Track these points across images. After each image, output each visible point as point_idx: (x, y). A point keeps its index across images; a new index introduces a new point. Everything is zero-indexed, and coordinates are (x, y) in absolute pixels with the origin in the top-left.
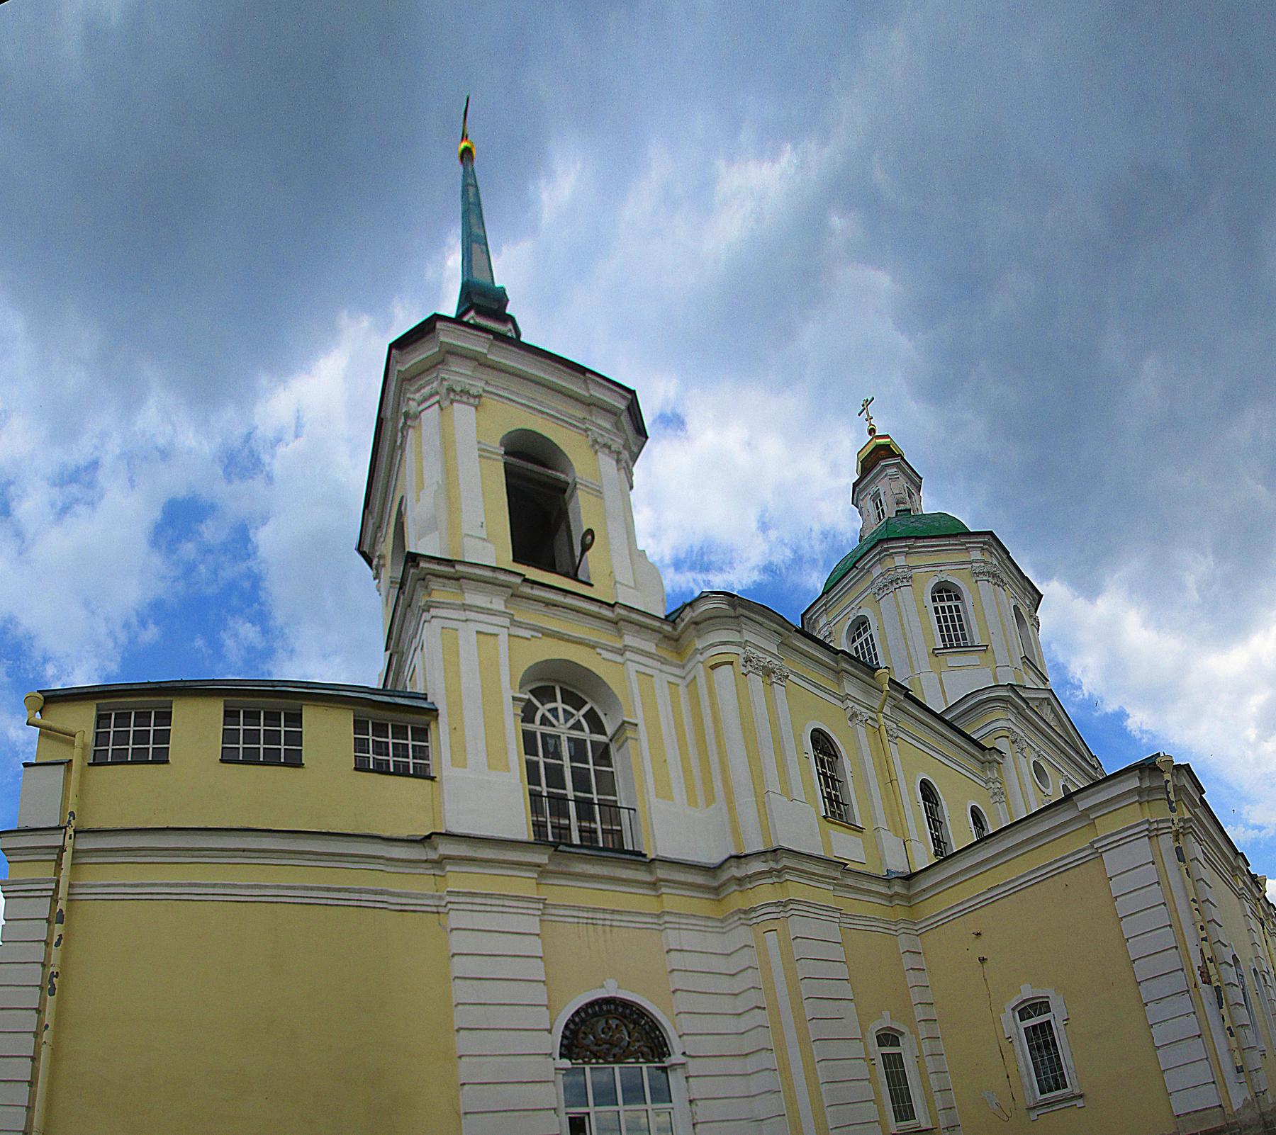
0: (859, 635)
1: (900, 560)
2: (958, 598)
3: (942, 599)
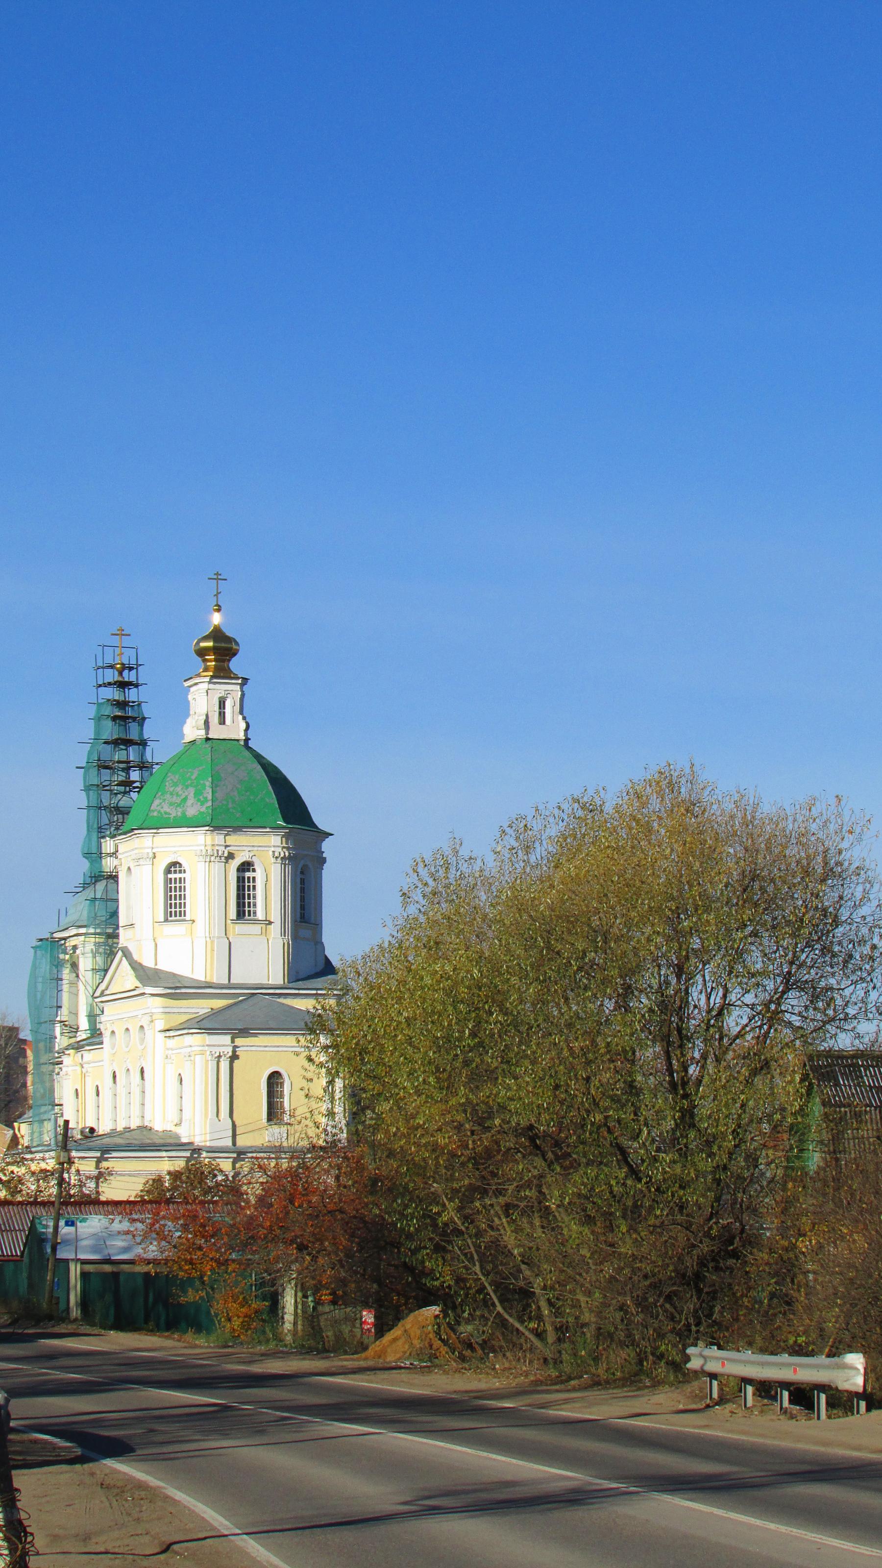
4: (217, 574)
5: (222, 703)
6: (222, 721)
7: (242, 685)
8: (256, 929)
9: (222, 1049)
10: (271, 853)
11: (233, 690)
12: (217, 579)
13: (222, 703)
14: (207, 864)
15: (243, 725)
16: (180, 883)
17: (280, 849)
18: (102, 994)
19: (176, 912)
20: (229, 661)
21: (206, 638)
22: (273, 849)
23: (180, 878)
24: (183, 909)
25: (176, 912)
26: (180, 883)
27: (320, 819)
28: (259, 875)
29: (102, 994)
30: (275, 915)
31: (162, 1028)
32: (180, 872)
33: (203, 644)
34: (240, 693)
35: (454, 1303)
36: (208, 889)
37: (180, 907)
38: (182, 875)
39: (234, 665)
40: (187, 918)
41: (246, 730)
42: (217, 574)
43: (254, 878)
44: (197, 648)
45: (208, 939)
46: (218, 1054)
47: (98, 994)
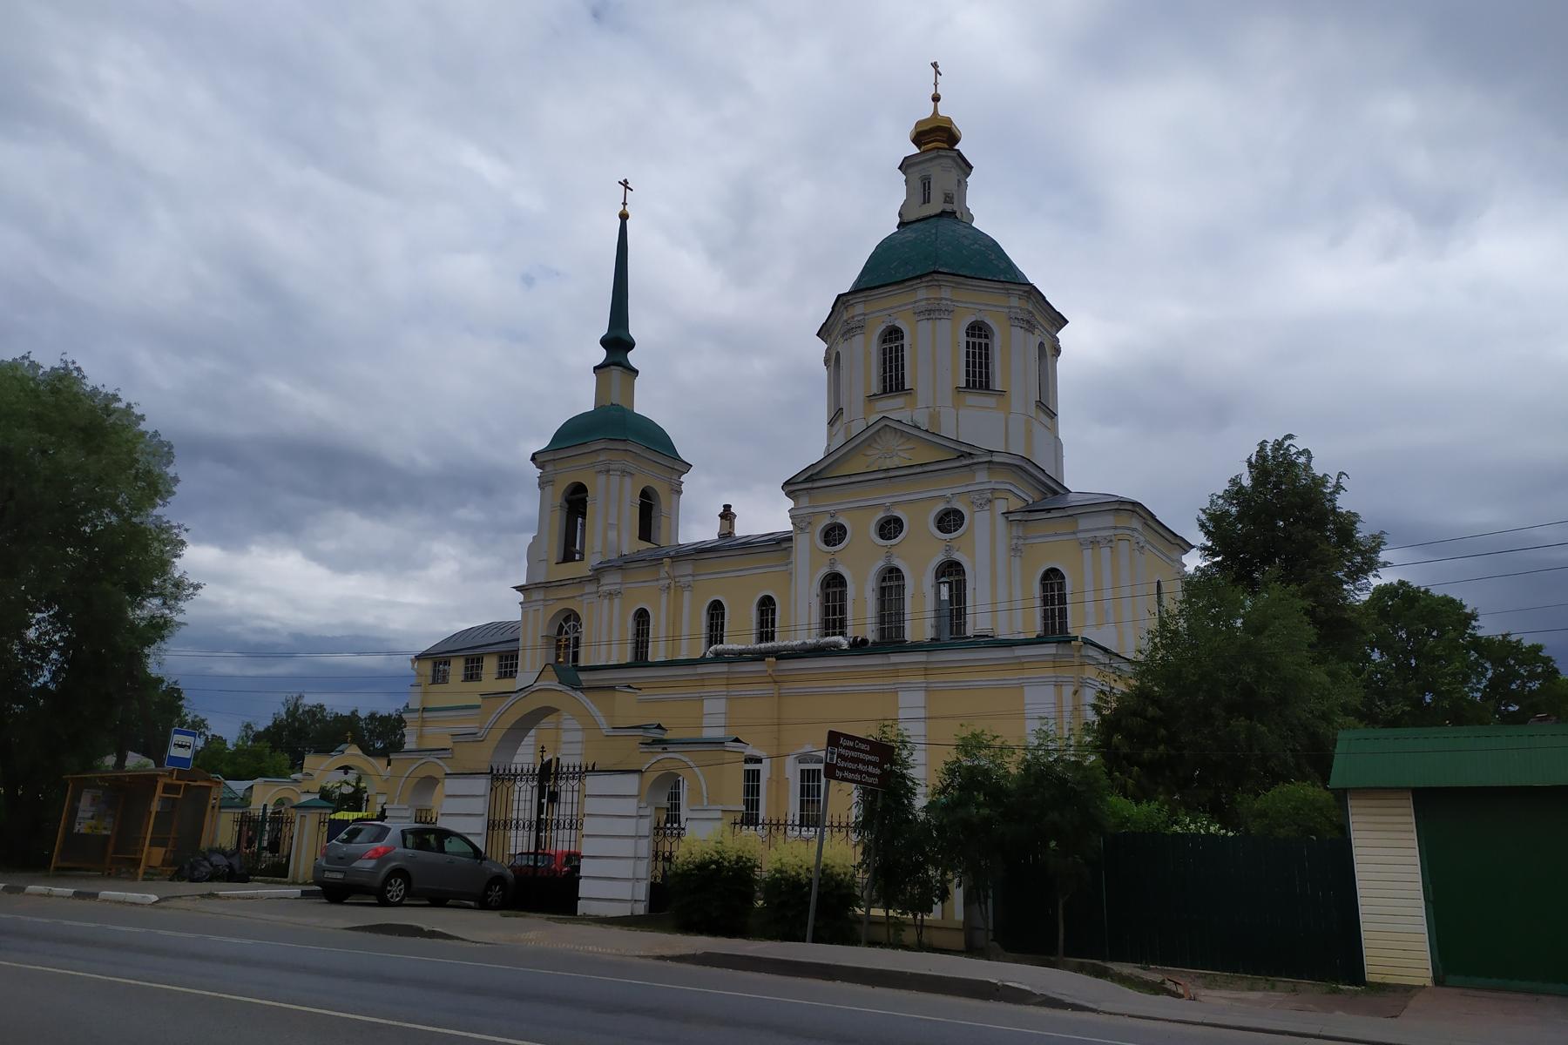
1: (946, 293)
2: (986, 337)
3: (973, 335)
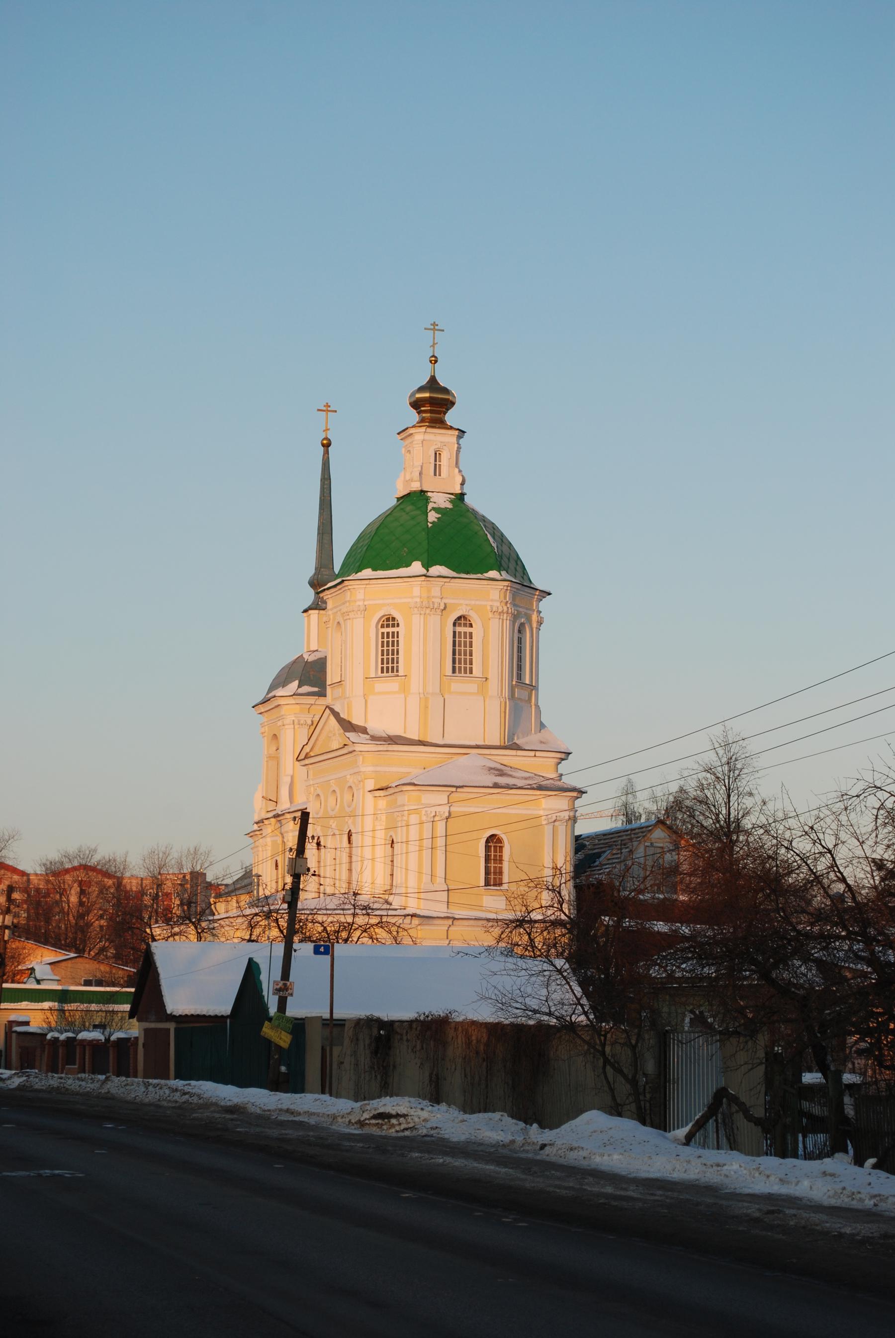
0: (388, 626)
4: (434, 324)
5: (437, 455)
6: (437, 471)
7: (459, 437)
8: (473, 687)
9: (438, 809)
10: (489, 608)
11: (446, 438)
12: (434, 330)
13: (437, 455)
14: (422, 617)
15: (460, 479)
16: (393, 637)
17: (498, 604)
18: (306, 757)
19: (388, 637)
20: (445, 413)
21: (421, 389)
22: (490, 603)
23: (393, 633)
24: (396, 639)
25: (388, 637)
26: (393, 637)
27: (538, 581)
28: (477, 631)
29: (306, 757)
30: (494, 673)
31: (372, 788)
32: (393, 626)
33: (418, 396)
34: (456, 446)
35: (721, 850)
36: (423, 645)
37: (393, 663)
38: (395, 629)
39: (450, 417)
40: (400, 673)
41: (462, 484)
42: (434, 324)
43: (471, 634)
44: (413, 399)
45: (422, 696)
46: (433, 814)
47: (302, 756)
